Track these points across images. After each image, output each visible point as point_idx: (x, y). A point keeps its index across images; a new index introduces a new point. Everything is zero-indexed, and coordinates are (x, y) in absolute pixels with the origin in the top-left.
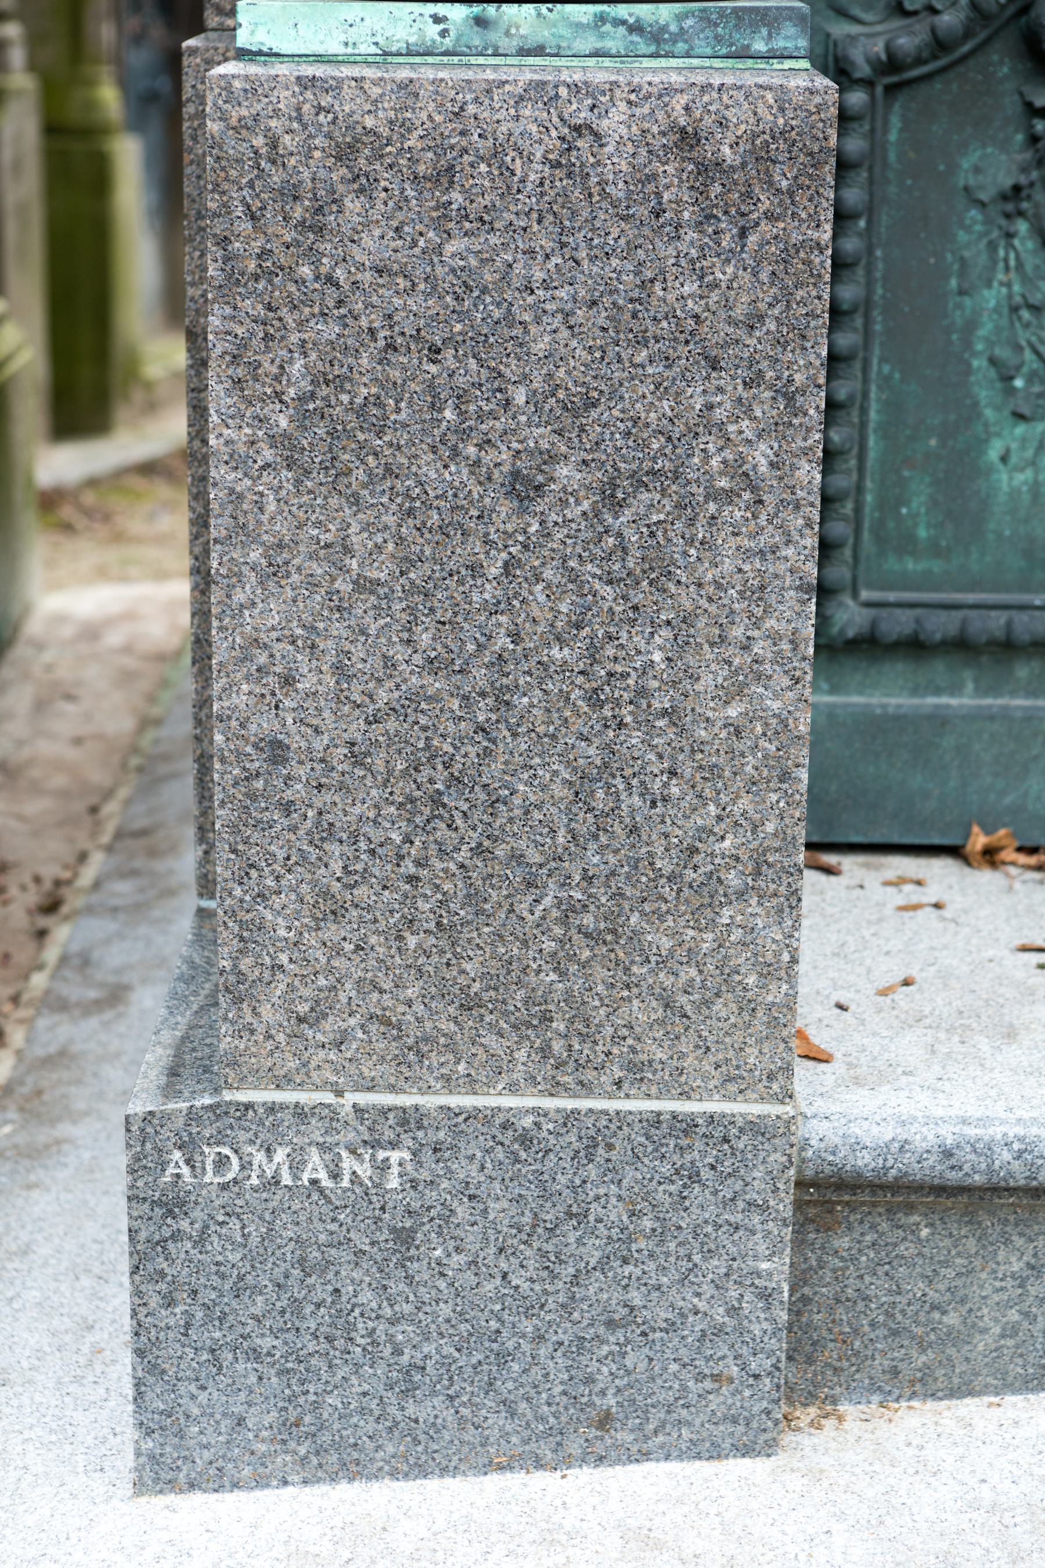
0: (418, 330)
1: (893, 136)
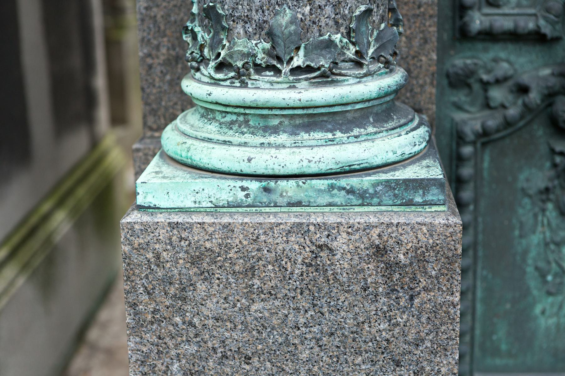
0: (239, 348)
1: (486, 164)
